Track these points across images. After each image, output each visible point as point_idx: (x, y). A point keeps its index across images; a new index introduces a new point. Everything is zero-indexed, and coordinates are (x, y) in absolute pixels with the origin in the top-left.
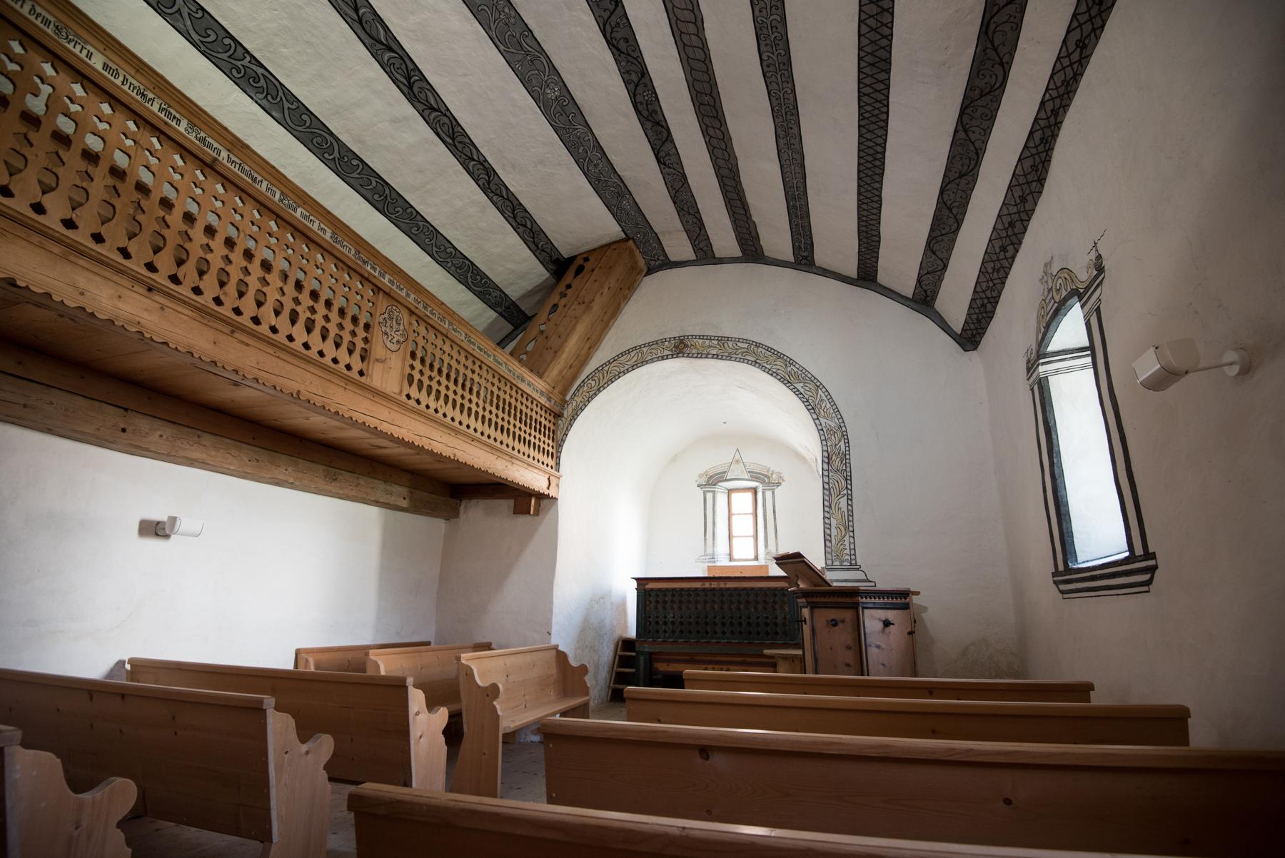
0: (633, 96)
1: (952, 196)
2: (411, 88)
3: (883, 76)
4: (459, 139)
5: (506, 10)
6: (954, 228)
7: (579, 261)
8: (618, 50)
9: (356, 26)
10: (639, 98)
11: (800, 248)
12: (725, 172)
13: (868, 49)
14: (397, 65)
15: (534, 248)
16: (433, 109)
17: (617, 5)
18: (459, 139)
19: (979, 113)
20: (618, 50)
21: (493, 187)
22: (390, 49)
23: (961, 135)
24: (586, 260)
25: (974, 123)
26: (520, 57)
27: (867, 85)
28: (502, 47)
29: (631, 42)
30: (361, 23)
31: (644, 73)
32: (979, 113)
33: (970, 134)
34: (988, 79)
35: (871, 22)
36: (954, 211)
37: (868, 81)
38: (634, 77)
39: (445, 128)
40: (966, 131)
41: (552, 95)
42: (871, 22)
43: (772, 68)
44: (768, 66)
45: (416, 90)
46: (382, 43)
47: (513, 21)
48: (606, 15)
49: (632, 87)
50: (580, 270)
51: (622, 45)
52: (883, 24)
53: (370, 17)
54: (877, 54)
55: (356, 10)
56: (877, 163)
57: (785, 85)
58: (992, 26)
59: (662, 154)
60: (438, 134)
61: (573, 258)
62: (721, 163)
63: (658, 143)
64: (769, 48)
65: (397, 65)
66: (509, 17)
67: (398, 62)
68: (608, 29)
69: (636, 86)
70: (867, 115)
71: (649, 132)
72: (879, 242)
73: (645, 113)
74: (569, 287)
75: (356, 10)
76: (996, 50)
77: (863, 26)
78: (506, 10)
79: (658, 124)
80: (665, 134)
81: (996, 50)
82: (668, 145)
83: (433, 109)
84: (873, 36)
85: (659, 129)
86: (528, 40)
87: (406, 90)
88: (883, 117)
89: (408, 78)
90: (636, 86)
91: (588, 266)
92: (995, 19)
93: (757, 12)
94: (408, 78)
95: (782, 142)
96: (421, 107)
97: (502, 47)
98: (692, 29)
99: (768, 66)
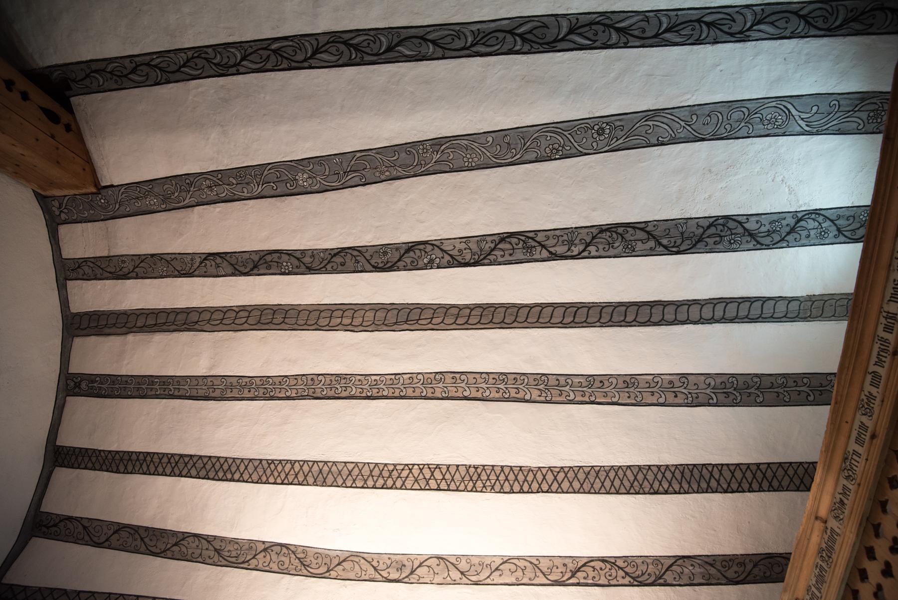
0: (290, 253)
1: (194, 545)
2: (345, 43)
3: (311, 480)
4: (273, 58)
5: (387, 173)
6: (154, 549)
7: (65, 118)
8: (335, 255)
9: (421, 32)
10: (285, 257)
11: (93, 382)
12: (194, 317)
13: (334, 469)
14: (372, 45)
15: (94, 66)
16: (316, 52)
17: (373, 267)
18: (273, 58)
19: (283, 559)
20: (335, 255)
21: (201, 62)
22: (389, 49)
23: (261, 547)
24: (68, 128)
25: (274, 557)
26: (345, 165)
27: (301, 467)
28: (359, 155)
29: (340, 268)
30: (422, 38)
31: (310, 270)
32: (283, 559)
33: (263, 554)
34: (314, 561)
35: (356, 472)
36: (176, 548)
37: (306, 468)
38: (307, 260)
39: (290, 51)
40: (265, 550)
41: (302, 178)
42: (356, 472)
43: (310, 382)
44: (312, 379)
45: (342, 47)
46: (397, 45)
47: (377, 174)
48: (367, 255)
49: (298, 255)
50: (53, 118)
51: (338, 259)
52: (354, 481)
53: (423, 50)
54: (330, 476)
55: (434, 42)
56: (221, 474)
57: (294, 391)
58: (357, 559)
59: (219, 260)
60: (286, 38)
61: (70, 110)
62: (206, 316)
63: (233, 261)
64: (328, 382)
65: (372, 45)
66: (382, 173)
67: (375, 48)
68: (355, 253)
69: (298, 259)
70: (272, 466)
71: (247, 256)
72: (118, 472)
73: (268, 258)
74: (25, 96)
75: (434, 42)
76: (339, 564)
77: (353, 465)
78: (387, 173)
79: (255, 267)
80: (242, 269)
81: (339, 564)
82: (230, 270)
83: (316, 52)
84: (345, 472)
85: (250, 266)
86: (357, 179)
87: (346, 36)
88: (271, 480)
89: (356, 47)
90: (298, 259)
91: (59, 130)
92: (363, 561)
93: (359, 377)
94: (356, 47)
95: (234, 380)
96: (323, 40)
97: (359, 155)
98: (346, 321)
99: (312, 379)
